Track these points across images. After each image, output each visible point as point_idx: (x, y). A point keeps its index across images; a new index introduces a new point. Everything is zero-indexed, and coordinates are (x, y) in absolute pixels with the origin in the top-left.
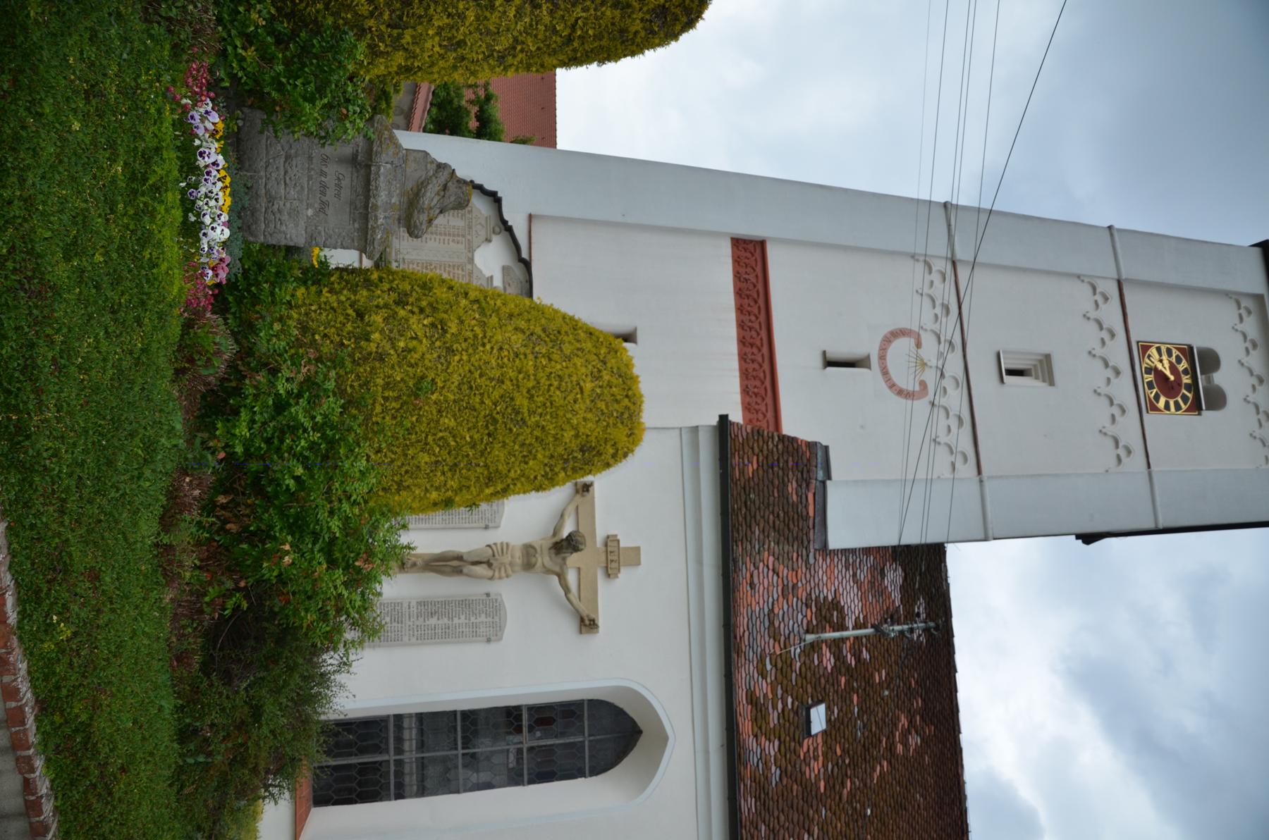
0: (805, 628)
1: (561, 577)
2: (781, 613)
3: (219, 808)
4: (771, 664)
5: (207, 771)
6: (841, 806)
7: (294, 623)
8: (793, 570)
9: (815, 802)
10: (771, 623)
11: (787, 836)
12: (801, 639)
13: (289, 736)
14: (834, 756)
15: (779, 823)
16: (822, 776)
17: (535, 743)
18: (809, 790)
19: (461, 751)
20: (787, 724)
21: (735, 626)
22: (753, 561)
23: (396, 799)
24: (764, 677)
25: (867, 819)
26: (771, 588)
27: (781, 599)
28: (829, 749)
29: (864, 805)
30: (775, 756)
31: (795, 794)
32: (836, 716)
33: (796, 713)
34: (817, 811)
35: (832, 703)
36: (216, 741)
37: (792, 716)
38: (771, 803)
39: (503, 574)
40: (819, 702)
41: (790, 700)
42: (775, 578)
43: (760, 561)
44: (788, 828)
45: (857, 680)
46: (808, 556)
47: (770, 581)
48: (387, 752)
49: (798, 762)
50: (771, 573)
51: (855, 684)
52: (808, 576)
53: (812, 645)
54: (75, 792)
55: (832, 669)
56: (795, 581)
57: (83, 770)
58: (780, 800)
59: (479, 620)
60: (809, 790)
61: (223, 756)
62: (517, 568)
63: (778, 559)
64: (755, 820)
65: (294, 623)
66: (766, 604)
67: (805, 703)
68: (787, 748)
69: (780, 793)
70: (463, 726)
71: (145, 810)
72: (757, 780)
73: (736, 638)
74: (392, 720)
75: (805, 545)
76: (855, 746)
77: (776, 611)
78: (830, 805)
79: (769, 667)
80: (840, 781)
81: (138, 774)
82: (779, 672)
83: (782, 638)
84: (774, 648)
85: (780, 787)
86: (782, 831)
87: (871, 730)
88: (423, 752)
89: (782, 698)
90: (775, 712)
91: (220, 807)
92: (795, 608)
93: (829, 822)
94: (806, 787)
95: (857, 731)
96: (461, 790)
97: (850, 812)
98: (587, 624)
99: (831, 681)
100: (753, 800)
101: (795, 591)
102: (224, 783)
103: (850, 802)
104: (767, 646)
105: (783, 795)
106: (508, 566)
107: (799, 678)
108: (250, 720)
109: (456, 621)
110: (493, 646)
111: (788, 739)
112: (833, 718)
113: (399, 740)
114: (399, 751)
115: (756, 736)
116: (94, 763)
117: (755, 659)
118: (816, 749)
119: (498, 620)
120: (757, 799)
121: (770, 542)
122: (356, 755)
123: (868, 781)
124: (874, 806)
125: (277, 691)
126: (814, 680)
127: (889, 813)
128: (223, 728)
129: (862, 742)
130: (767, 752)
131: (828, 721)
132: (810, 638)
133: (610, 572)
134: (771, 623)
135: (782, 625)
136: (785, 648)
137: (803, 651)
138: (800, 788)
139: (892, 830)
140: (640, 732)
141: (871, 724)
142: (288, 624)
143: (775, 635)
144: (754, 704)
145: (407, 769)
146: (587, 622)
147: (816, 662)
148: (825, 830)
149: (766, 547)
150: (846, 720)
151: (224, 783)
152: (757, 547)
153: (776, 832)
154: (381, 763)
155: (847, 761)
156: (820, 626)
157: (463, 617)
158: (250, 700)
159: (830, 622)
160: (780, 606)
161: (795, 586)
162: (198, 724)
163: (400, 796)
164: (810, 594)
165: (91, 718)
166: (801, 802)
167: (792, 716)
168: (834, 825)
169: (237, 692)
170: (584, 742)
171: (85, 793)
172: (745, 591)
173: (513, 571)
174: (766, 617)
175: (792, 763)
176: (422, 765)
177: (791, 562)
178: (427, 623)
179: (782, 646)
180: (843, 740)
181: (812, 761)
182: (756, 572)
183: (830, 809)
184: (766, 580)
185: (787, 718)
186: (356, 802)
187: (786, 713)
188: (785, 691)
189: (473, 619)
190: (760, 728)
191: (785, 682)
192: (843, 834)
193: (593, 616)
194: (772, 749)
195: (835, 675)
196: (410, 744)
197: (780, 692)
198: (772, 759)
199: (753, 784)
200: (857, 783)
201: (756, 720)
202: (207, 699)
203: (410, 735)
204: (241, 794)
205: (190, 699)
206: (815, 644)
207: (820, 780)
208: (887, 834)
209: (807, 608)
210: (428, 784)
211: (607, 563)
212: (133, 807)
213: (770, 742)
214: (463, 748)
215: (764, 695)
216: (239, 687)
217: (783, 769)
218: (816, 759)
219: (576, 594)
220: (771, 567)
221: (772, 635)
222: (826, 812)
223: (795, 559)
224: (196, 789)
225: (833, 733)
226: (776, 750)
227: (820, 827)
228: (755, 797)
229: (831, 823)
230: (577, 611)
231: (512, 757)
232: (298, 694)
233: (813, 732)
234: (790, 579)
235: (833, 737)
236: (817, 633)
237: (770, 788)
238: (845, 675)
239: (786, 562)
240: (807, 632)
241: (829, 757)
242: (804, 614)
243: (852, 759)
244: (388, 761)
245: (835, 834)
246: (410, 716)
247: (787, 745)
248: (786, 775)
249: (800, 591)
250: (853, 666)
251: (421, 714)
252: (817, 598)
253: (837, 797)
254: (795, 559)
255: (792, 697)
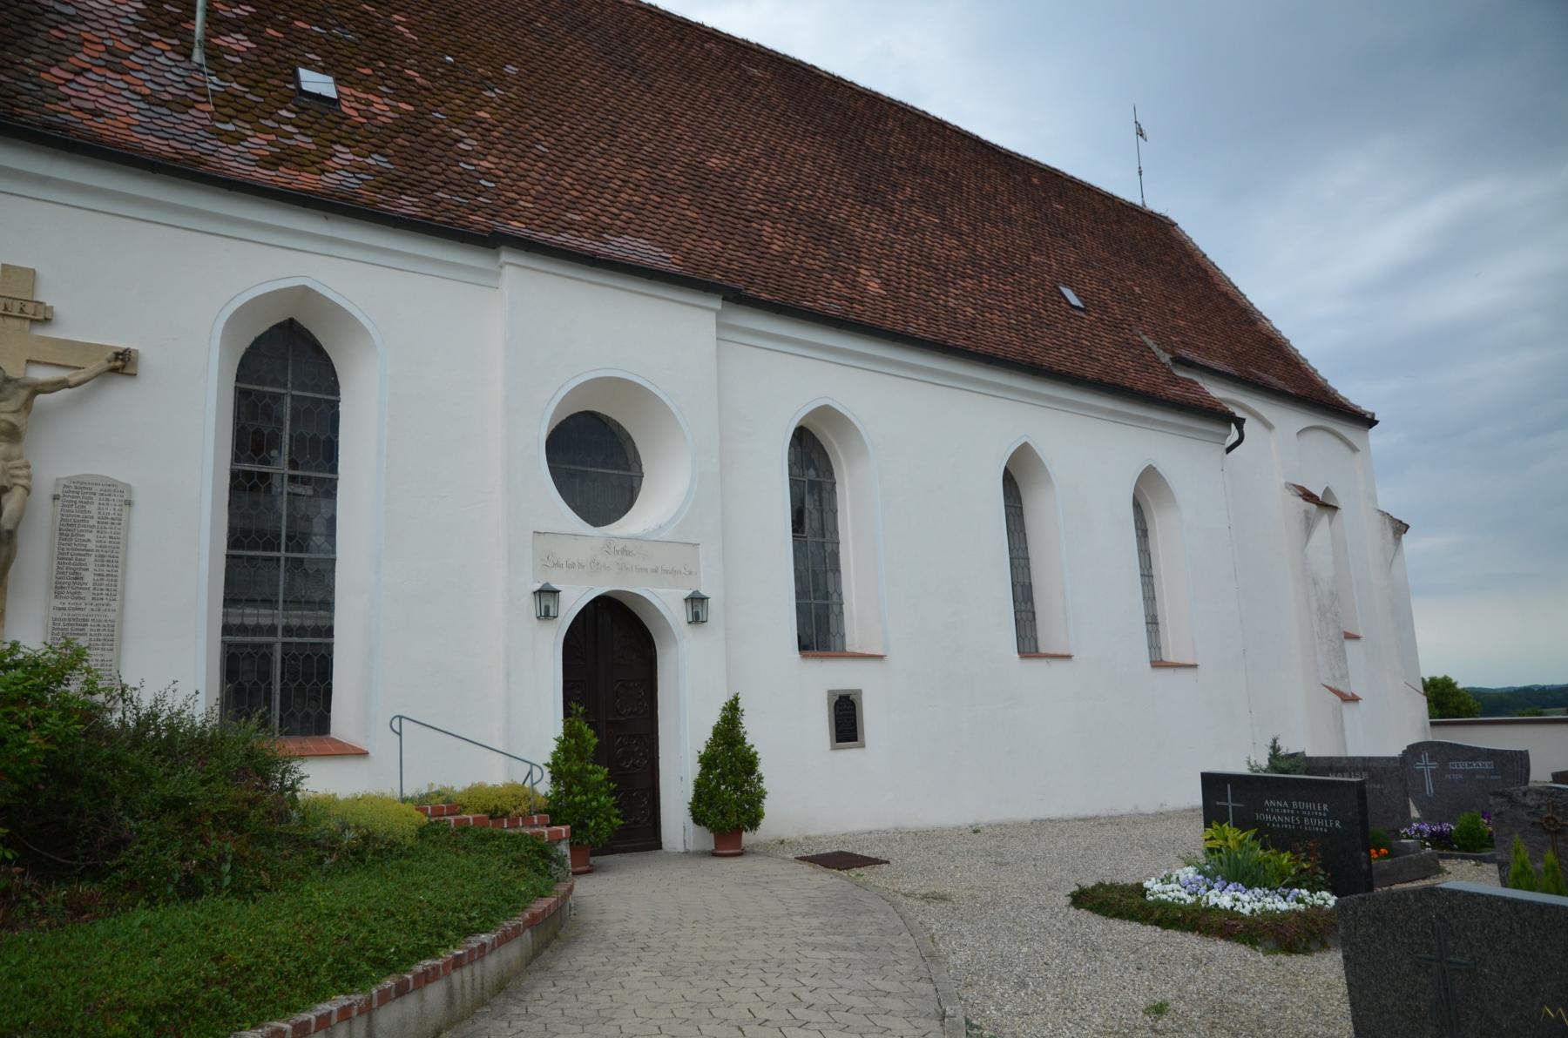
0: (182, 58)
1: (38, 389)
2: (149, 85)
3: (298, 840)
4: (227, 123)
5: (245, 860)
6: (435, 91)
7: (39, 762)
8: (81, 44)
9: (424, 122)
10: (164, 104)
11: (455, 169)
12: (197, 70)
13: (215, 762)
14: (372, 79)
15: (439, 174)
16: (394, 103)
17: (285, 459)
18: (406, 125)
19: (283, 554)
20: (316, 126)
21: (158, 155)
22: (54, 100)
23: (333, 636)
24: (244, 138)
25: (458, 64)
26: (107, 87)
27: (127, 78)
28: (359, 82)
29: (442, 63)
30: (354, 154)
31: (408, 144)
32: (319, 59)
33: (304, 110)
34: (435, 122)
35: (299, 58)
36: (205, 852)
37: (306, 117)
38: (412, 176)
39: (23, 472)
40: (296, 78)
41: (284, 113)
42: (90, 75)
43: (56, 89)
44: (447, 165)
45: (275, 13)
46: (60, 13)
47: (94, 84)
48: (270, 646)
49: (369, 127)
50: (81, 80)
51: (281, 18)
52: (95, 25)
53: (208, 57)
54: (237, 1009)
55: (252, 42)
56: (102, 48)
57: (209, 1006)
58: (411, 164)
59: (95, 513)
60: (406, 125)
61: (227, 842)
62: (15, 450)
63: (57, 61)
64: (427, 201)
65: (39, 762)
66: (131, 102)
67: (293, 94)
68: (347, 135)
69: (403, 162)
70: (250, 548)
71: (278, 927)
72: (381, 185)
73: (175, 160)
74: (228, 638)
75: (40, 11)
76: (364, 47)
77: (148, 92)
78: (484, 129)
79: (230, 127)
80: (405, 83)
81: (228, 939)
82: (240, 115)
83: (191, 95)
84: (203, 112)
85: (396, 160)
86: (449, 173)
87: (349, 19)
88: (277, 601)
89: (279, 123)
90: (295, 136)
91: (300, 843)
92: (147, 63)
93: (451, 113)
94: (403, 128)
95: (345, 38)
96: (331, 556)
97: (446, 83)
98: (122, 364)
99: (269, 49)
100: (403, 197)
101: (119, 53)
102: (266, 839)
103: (434, 79)
104: (198, 121)
105: (405, 159)
106: (10, 464)
107: (255, 92)
108: (182, 813)
109: (91, 546)
110: (138, 498)
111: (336, 131)
112: (321, 64)
113: (257, 630)
114: (272, 630)
115: (323, 171)
116: (201, 994)
117: (214, 142)
118: (357, 99)
119: (98, 488)
120: (402, 191)
121: (22, 63)
122: (270, 684)
123: (414, 46)
124: (445, 51)
125: (146, 780)
126: (262, 72)
127: (457, 34)
128: (189, 845)
129: (361, 36)
130: (348, 163)
131: (323, 71)
132: (198, 56)
133: (40, 317)
134: (164, 104)
135: (170, 89)
136: (206, 96)
137: (217, 73)
138: (403, 135)
139: (479, 39)
140: (291, 321)
141: (340, 15)
142: (43, 770)
143: (183, 105)
144: (279, 162)
145: (295, 622)
146: (119, 363)
147: (237, 60)
148: (459, 121)
149: (31, 72)
150: (328, 47)
151: (266, 839)
152: (30, 86)
153: (448, 181)
154: (285, 654)
155: (382, 65)
156: (183, 37)
157: (88, 536)
158: (153, 814)
159: (179, 20)
160: (141, 83)
161: (109, 50)
162: (177, 877)
163: (329, 632)
164: (128, 32)
165: (135, 1010)
166: (419, 139)
167: (306, 117)
168: (456, 108)
169: (139, 831)
170: (293, 396)
171: (240, 998)
172: (105, 126)
173: (19, 457)
174: (154, 108)
175: (369, 135)
176: (293, 602)
177: (66, 43)
178: (90, 585)
179: (204, 99)
180: (353, 61)
181: (372, 109)
182: (74, 101)
183: (437, 106)
184: (92, 91)
185: (309, 125)
186: (330, 684)
187: (300, 123)
188: (270, 115)
189: (93, 522)
190: (314, 163)
191: (257, 111)
192: (469, 100)
193: (110, 354)
194: (344, 155)
195: (262, 41)
196: (262, 616)
197: (269, 123)
198: (357, 158)
199: (384, 191)
200: (412, 61)
201: (300, 165)
202: (142, 869)
203: (252, 616)
204: (283, 817)
205: (143, 888)
206: (209, 52)
207: (398, 107)
208: (481, 47)
209: (150, 45)
210: (317, 596)
211: (25, 318)
212: (271, 940)
213: (335, 156)
214: (279, 550)
215: (269, 144)
216: (131, 830)
217: (374, 149)
218: (370, 103)
219: (73, 372)
220: (70, 76)
221: (183, 109)
222: (438, 112)
223: (63, 36)
224: (266, 870)
225: (340, 69)
226: (347, 150)
227: (454, 125)
228: (400, 194)
229: (453, 110)
230: (98, 375)
231: (300, 490)
232: (156, 753)
233: (334, 95)
234: (97, 55)
235: (348, 72)
236: (193, 43)
237: (393, 172)
238: (265, 27)
239: (64, 50)
240: (188, 57)
241: (371, 85)
242: (159, 52)
243: (380, 57)
244: (284, 644)
245: (467, 109)
246: (225, 615)
247: (343, 134)
248: (383, 148)
249: (118, 45)
250: (254, 10)
251: (225, 600)
252: (135, 23)
253: (424, 92)
254: (63, 36)
255: (281, 109)
